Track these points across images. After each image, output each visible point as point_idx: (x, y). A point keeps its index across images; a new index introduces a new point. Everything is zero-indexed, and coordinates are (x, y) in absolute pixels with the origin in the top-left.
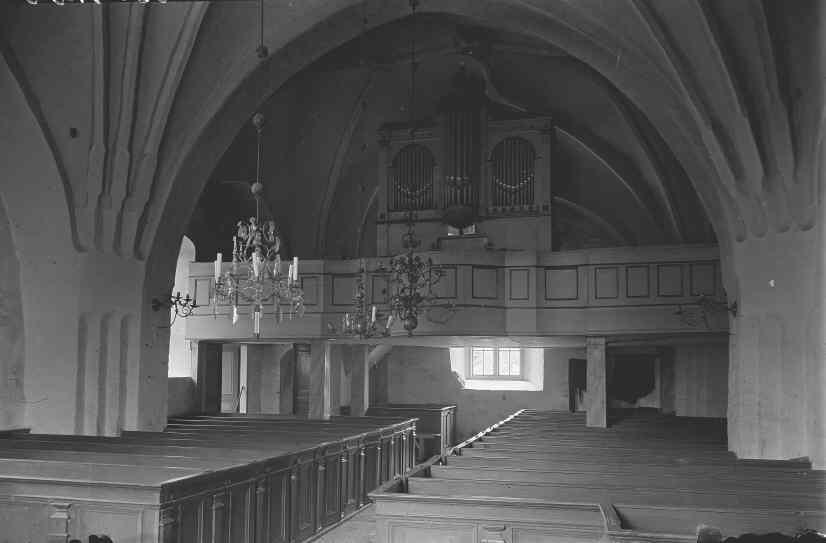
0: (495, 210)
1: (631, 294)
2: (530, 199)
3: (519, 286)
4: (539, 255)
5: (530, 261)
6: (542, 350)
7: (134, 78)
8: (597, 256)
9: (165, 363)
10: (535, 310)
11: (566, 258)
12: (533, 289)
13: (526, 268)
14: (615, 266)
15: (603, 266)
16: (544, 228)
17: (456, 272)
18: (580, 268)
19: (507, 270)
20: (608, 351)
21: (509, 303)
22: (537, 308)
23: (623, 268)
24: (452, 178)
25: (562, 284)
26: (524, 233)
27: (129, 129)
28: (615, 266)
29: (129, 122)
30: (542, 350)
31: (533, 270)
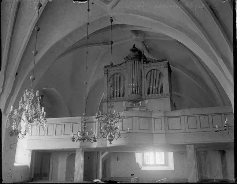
0: (148, 96)
1: (202, 126)
2: (161, 91)
3: (158, 124)
4: (165, 112)
5: (161, 114)
6: (173, 153)
7: (7, 51)
8: (187, 112)
9: (14, 158)
10: (164, 134)
11: (177, 113)
12: (163, 125)
13: (160, 118)
14: (194, 115)
15: (188, 116)
16: (166, 104)
17: (132, 119)
18: (181, 117)
19: (153, 119)
20: (195, 149)
21: (154, 131)
22: (165, 133)
23: (210, 116)
24: (131, 84)
25: (175, 123)
26: (159, 105)
27: (7, 71)
28: (194, 115)
29: (146, 131)
30: (173, 153)
31: (163, 119)
